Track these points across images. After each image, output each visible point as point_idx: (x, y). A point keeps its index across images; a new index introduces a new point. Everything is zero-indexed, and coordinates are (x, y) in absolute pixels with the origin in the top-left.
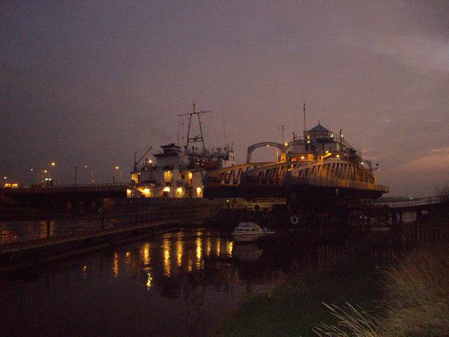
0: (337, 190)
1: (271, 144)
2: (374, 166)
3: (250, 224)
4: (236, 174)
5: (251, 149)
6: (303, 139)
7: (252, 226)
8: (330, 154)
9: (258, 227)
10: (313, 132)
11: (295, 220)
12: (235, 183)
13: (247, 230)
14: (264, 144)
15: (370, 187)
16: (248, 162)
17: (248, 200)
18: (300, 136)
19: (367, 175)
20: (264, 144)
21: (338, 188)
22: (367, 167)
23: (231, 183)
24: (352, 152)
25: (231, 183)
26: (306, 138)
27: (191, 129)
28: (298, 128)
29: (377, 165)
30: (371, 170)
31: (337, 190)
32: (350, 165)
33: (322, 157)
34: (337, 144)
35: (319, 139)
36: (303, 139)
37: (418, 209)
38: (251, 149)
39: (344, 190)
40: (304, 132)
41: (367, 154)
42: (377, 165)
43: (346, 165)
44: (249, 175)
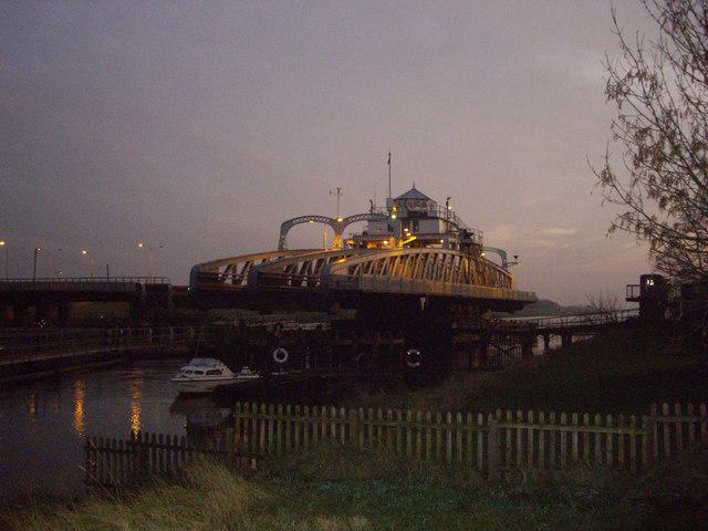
0: (423, 300)
1: (317, 219)
2: (510, 259)
3: (207, 360)
4: (239, 271)
5: (287, 226)
6: (385, 211)
7: (213, 364)
8: (413, 238)
9: (221, 366)
10: (401, 201)
11: (281, 356)
12: (235, 282)
13: (198, 372)
14: (304, 219)
15: (497, 293)
16: (281, 247)
17: (264, 312)
18: (381, 206)
19: (500, 274)
20: (304, 219)
21: (424, 295)
22: (498, 260)
23: (304, 284)
24: (466, 234)
25: (304, 284)
26: (390, 211)
27: (387, 180)
28: (369, 192)
29: (516, 257)
30: (505, 265)
31: (423, 300)
32: (461, 257)
33: (401, 243)
34: (441, 222)
35: (414, 210)
36: (385, 211)
37: (565, 332)
38: (287, 226)
39: (435, 300)
40: (388, 199)
41: (494, 237)
42: (516, 257)
43: (453, 256)
44: (266, 270)
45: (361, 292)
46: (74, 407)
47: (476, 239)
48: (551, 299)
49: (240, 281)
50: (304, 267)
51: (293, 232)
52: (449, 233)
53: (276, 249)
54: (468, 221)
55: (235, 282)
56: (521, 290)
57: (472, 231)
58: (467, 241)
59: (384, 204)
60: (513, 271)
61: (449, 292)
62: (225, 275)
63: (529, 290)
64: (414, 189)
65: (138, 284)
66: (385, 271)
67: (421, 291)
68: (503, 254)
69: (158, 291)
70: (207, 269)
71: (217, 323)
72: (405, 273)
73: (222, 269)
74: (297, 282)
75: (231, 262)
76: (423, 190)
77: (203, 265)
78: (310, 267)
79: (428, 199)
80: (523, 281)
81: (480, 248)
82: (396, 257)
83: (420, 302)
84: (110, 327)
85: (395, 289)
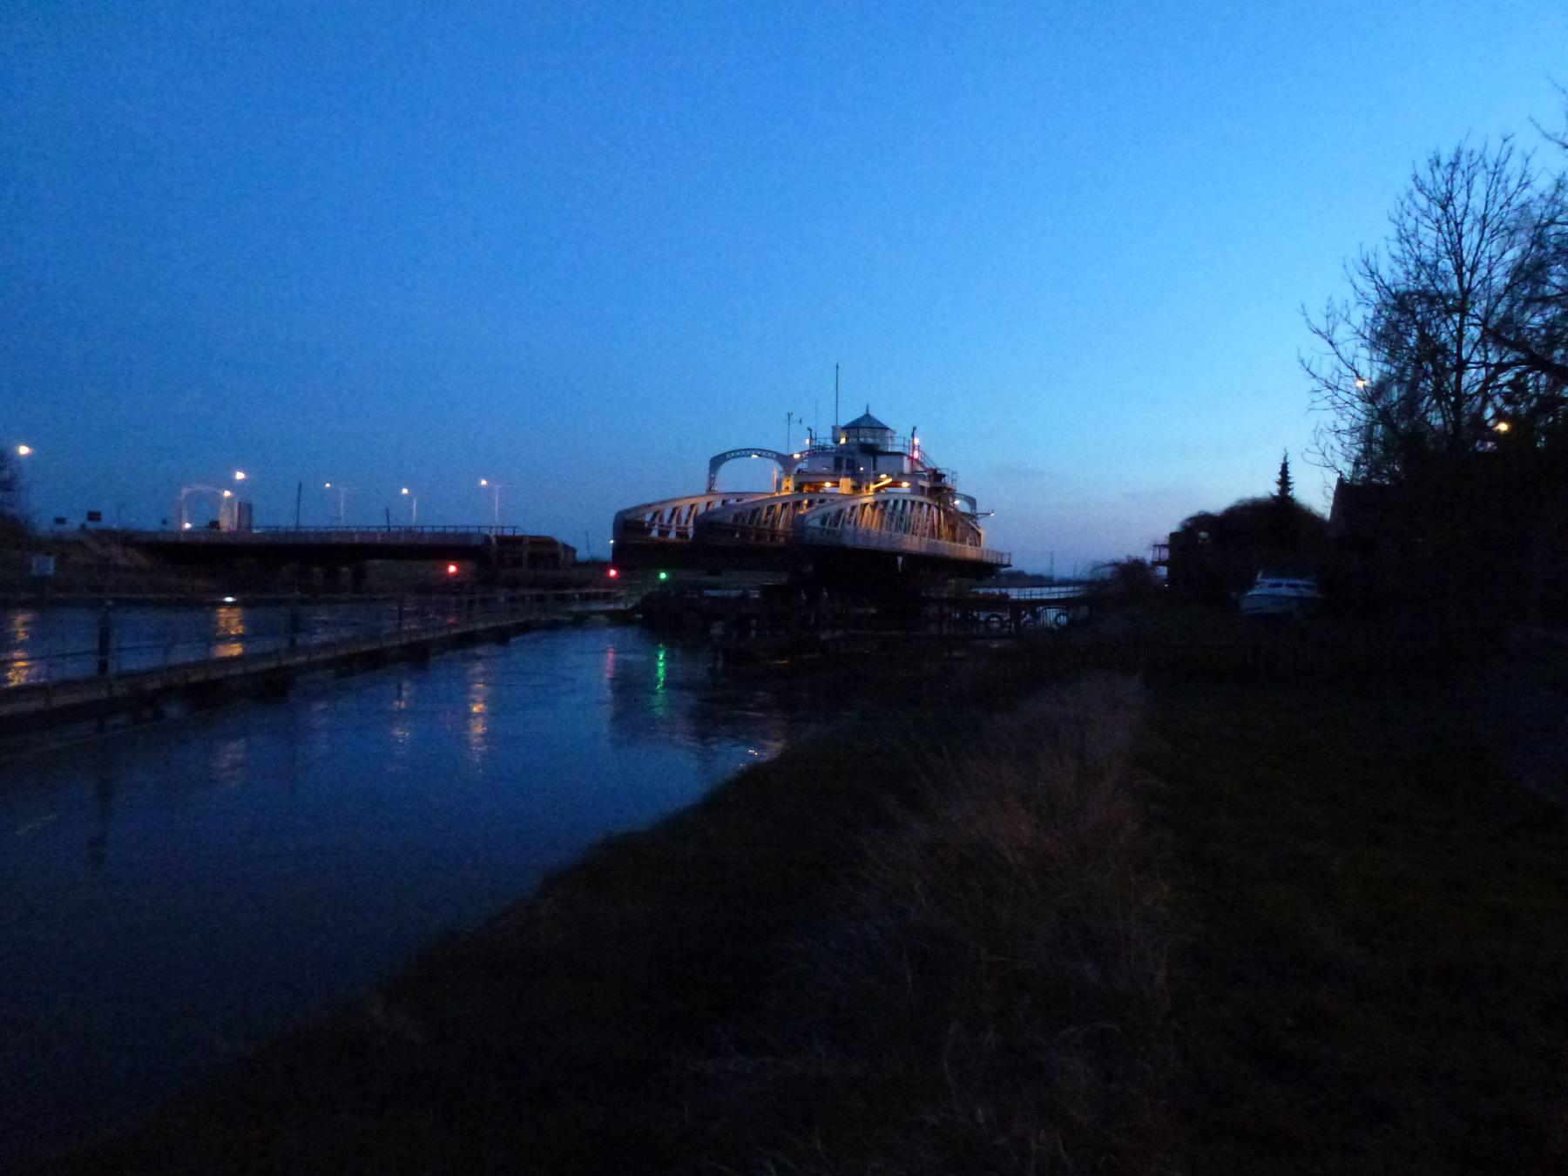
0: (900, 559)
1: (762, 453)
2: (981, 508)
4: (684, 516)
5: (717, 462)
14: (746, 452)
15: (970, 552)
20: (746, 452)
24: (937, 476)
27: (834, 395)
31: (900, 559)
32: (929, 506)
34: (905, 458)
38: (717, 462)
45: (844, 547)
46: (668, 671)
47: (948, 481)
48: (562, 537)
49: (668, 533)
50: (672, 515)
51: (726, 468)
53: (704, 492)
55: (661, 533)
57: (945, 472)
58: (938, 485)
59: (829, 433)
60: (984, 528)
61: (924, 549)
63: (999, 548)
65: (487, 538)
68: (971, 501)
69: (1131, 572)
70: (633, 515)
72: (874, 524)
73: (648, 518)
74: (664, 533)
77: (628, 511)
78: (679, 515)
80: (994, 539)
81: (952, 493)
82: (866, 505)
83: (897, 561)
84: (454, 594)
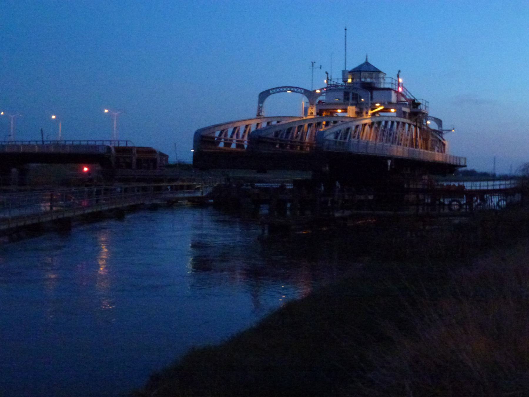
0: (389, 162)
1: (294, 89)
2: (445, 126)
5: (264, 95)
14: (282, 89)
16: (259, 115)
20: (282, 89)
21: (390, 158)
24: (414, 104)
25: (233, 146)
31: (389, 162)
34: (393, 92)
38: (264, 95)
39: (399, 162)
45: (350, 153)
47: (422, 107)
49: (230, 144)
51: (269, 100)
52: (399, 103)
54: (163, 151)
56: (452, 154)
57: (420, 101)
58: (415, 110)
59: (340, 76)
60: (447, 138)
62: (219, 139)
64: (367, 63)
65: (109, 148)
66: (359, 136)
67: (388, 154)
68: (439, 122)
70: (206, 133)
71: (298, 233)
73: (217, 134)
75: (222, 128)
76: (374, 62)
79: (380, 72)
81: (426, 116)
83: (387, 163)
85: (362, 151)
